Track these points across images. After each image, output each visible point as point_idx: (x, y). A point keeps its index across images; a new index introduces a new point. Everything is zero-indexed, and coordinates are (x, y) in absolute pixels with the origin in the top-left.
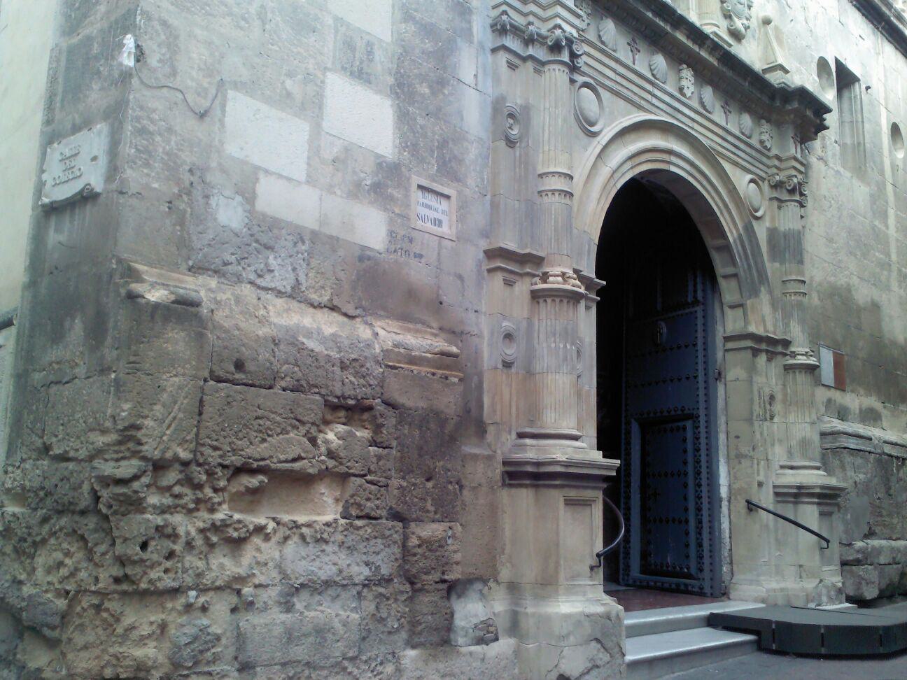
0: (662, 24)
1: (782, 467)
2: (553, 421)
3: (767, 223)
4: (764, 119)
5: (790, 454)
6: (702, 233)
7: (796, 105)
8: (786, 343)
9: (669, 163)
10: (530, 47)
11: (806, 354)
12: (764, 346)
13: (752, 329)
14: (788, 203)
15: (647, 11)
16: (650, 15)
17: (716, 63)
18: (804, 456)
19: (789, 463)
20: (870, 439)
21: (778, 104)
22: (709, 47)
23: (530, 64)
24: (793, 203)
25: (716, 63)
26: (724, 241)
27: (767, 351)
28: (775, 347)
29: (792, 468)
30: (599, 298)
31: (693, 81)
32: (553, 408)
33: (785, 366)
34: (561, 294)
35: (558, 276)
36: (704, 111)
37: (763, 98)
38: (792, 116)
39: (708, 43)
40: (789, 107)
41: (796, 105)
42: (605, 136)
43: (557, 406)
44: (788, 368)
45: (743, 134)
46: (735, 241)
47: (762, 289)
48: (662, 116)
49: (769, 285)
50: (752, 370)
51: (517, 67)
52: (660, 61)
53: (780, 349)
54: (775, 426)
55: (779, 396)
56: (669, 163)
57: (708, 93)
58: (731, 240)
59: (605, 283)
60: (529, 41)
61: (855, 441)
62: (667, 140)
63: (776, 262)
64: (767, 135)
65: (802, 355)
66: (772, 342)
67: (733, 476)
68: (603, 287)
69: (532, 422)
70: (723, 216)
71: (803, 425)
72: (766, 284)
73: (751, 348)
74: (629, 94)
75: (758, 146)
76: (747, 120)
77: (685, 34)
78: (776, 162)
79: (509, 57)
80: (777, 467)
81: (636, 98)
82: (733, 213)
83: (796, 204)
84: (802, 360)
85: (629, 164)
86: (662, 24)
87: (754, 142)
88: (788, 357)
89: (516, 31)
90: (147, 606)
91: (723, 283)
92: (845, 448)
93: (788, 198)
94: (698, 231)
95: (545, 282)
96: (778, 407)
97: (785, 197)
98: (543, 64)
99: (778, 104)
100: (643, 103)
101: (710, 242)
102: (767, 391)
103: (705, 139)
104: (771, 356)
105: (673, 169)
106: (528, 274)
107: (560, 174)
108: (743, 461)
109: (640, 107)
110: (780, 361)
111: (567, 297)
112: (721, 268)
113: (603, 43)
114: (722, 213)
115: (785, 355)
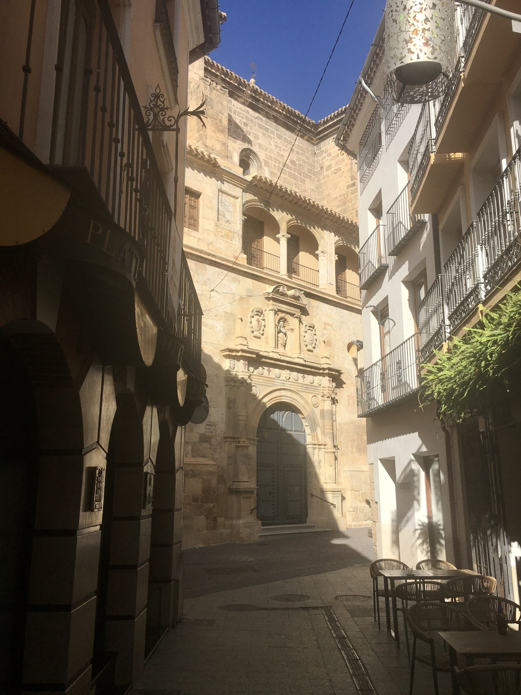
12: (317, 446)
105: (283, 400)
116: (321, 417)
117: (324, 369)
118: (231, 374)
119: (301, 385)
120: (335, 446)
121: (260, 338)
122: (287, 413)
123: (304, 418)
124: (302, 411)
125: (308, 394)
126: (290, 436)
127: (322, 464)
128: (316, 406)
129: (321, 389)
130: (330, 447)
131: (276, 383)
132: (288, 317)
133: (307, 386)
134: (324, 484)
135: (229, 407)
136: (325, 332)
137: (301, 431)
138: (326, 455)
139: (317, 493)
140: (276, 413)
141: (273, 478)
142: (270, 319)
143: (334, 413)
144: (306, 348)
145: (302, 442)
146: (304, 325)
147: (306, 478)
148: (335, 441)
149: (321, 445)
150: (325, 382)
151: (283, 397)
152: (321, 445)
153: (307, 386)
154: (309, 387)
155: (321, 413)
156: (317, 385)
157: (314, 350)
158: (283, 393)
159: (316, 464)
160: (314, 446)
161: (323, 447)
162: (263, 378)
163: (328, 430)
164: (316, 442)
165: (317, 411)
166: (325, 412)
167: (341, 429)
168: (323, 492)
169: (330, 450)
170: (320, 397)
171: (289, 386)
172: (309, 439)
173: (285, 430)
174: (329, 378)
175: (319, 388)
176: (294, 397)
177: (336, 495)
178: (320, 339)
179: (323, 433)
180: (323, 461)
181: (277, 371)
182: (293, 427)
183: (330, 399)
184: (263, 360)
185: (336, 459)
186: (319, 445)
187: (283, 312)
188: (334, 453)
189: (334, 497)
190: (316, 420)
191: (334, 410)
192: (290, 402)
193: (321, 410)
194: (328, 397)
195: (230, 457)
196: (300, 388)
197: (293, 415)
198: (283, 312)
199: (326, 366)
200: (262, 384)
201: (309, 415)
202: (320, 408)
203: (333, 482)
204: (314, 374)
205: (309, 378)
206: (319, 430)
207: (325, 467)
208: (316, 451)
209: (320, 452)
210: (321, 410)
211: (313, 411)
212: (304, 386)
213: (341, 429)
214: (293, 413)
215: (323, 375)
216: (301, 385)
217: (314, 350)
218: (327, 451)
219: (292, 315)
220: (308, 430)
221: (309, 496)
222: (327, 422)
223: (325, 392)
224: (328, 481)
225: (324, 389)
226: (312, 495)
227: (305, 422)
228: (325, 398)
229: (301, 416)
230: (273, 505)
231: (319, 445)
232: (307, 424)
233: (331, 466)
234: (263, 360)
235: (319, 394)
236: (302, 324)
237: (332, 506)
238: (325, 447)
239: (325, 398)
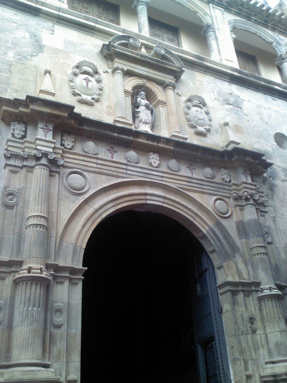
0: (125, 137)
1: (267, 363)
3: (235, 219)
4: (222, 167)
5: (270, 353)
6: (191, 231)
7: (236, 157)
8: (258, 284)
9: (146, 200)
10: (25, 162)
11: (270, 289)
12: (240, 288)
13: (230, 279)
14: (247, 206)
15: (113, 133)
16: (116, 135)
17: (172, 148)
18: (279, 354)
19: (270, 360)
20: (230, 337)
21: (226, 159)
22: (163, 141)
23: (24, 170)
24: (249, 206)
25: (172, 148)
26: (202, 233)
27: (243, 291)
28: (250, 288)
29: (273, 363)
30: (83, 278)
31: (158, 158)
33: (258, 297)
34: (24, 279)
36: (174, 172)
37: (216, 158)
38: (238, 163)
39: (162, 140)
40: (234, 159)
41: (236, 157)
42: (90, 193)
43: (24, 345)
44: (260, 299)
45: (206, 178)
46: (207, 231)
47: (236, 255)
48: (136, 178)
49: (240, 253)
50: (234, 303)
52: (132, 154)
53: (253, 288)
54: (258, 337)
55: (258, 318)
56: (146, 200)
57: (173, 163)
58: (205, 232)
59: (87, 268)
60: (24, 159)
62: (152, 191)
63: (243, 239)
64: (226, 175)
65: (267, 289)
66: (249, 285)
67: (235, 374)
68: (87, 271)
69: (8, 358)
71: (275, 333)
72: (238, 252)
73: (230, 291)
74: (105, 171)
75: (221, 181)
76: (208, 171)
77: (144, 139)
78: (235, 187)
80: (263, 363)
81: (115, 173)
82: (203, 217)
83: (251, 206)
84: (267, 292)
85: (111, 204)
86: (125, 137)
87: (217, 180)
88: (260, 292)
89: (15, 156)
91: (212, 256)
93: (245, 204)
94: (189, 231)
95: (29, 272)
96: (258, 324)
97: (244, 203)
98: (33, 167)
99: (226, 159)
100: (120, 174)
101: (197, 236)
102: (246, 316)
104: (248, 294)
105: (149, 202)
106: (12, 272)
107: (34, 216)
108: (237, 362)
110: (255, 295)
111: (30, 280)
112: (208, 249)
113: (86, 152)
114: (194, 219)
115: (258, 291)
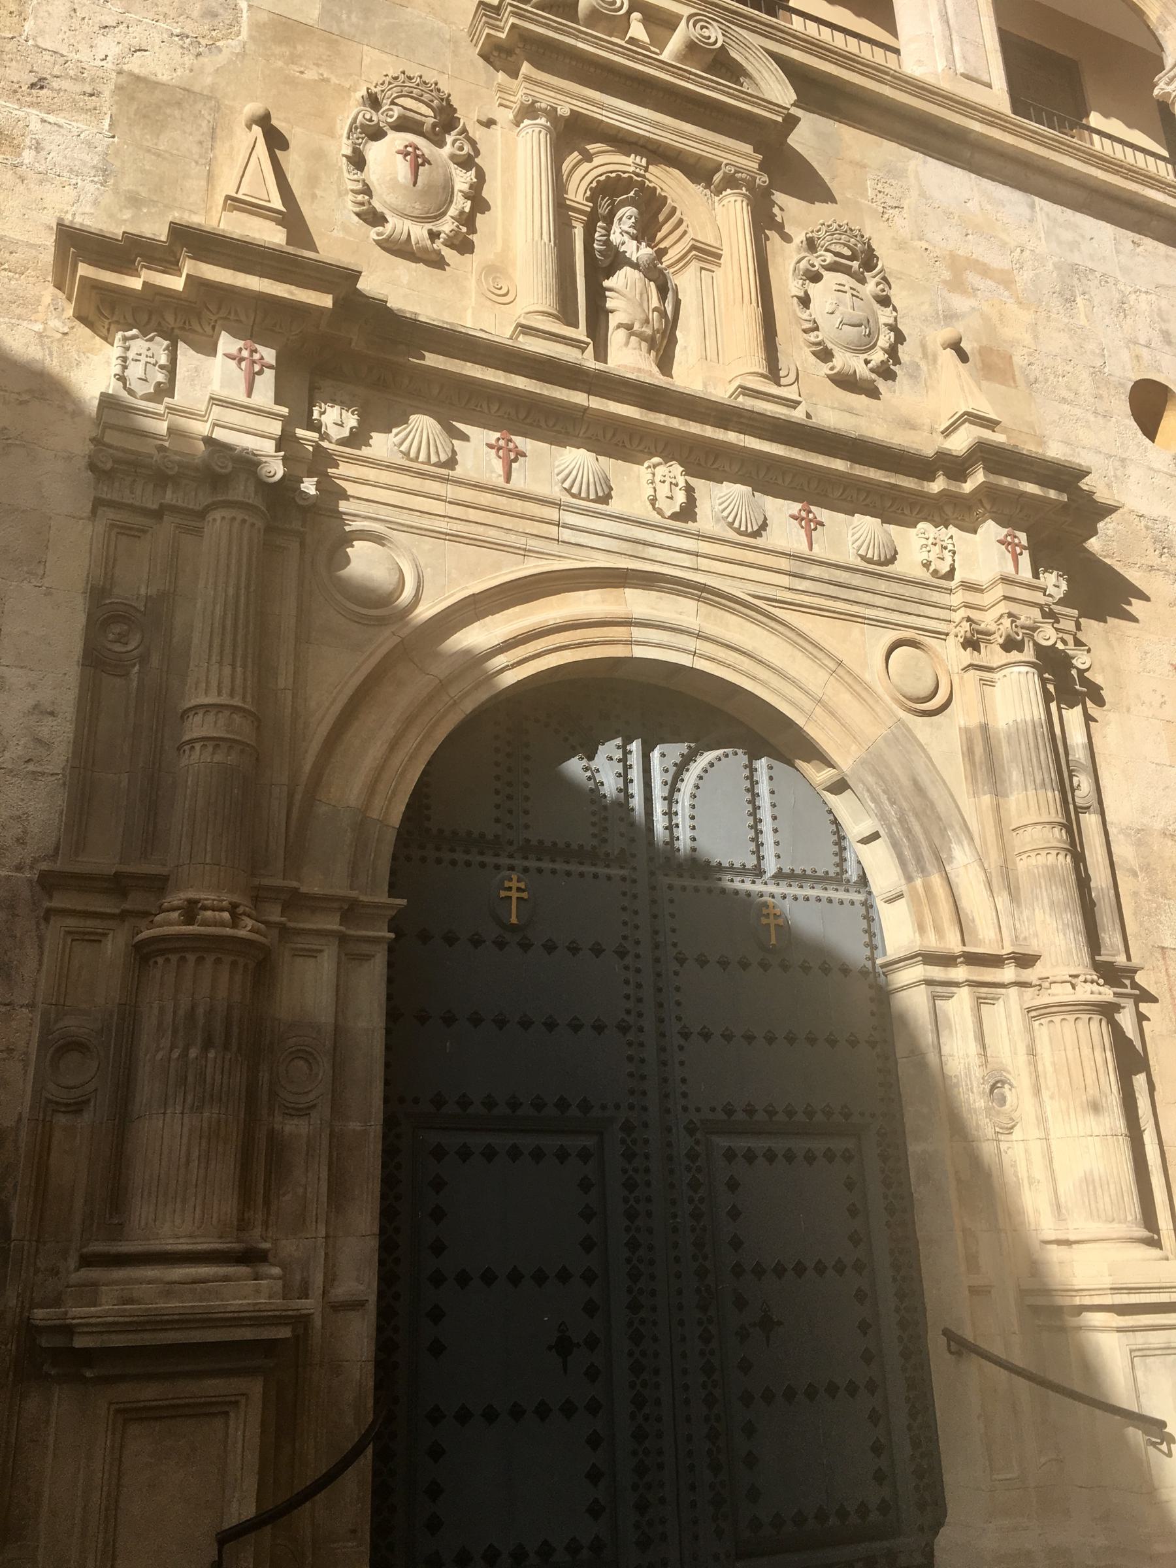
2: (143, 1223)
9: (630, 643)
12: (960, 973)
14: (1006, 671)
24: (1016, 669)
32: (1098, 1185)
35: (222, 910)
51: (144, 532)
56: (630, 643)
59: (404, 902)
61: (1043, 718)
68: (402, 911)
70: (764, 684)
79: (111, 516)
90: (767, 1323)
92: (835, 822)
100: (533, 544)
103: (729, 581)
105: (639, 652)
109: (526, 552)
116: (973, 779)
117: (957, 467)
118: (144, 434)
119: (784, 564)
120: (1110, 974)
121: (439, 263)
122: (710, 756)
123: (840, 786)
124: (812, 731)
125: (856, 629)
126: (749, 906)
127: (1019, 1097)
128: (929, 705)
129: (956, 599)
130: (1063, 972)
131: (566, 535)
132: (668, 182)
133: (843, 576)
134: (1056, 1254)
135: (96, 660)
136: (960, 303)
137: (837, 879)
138: (1042, 1030)
139: (998, 1328)
140: (610, 748)
141: (587, 1215)
142: (518, 163)
143: (1079, 754)
144: (825, 369)
145: (853, 949)
146: (799, 237)
147: (901, 1207)
148: (1110, 938)
149: (995, 961)
150: (985, 553)
151: (637, 633)
152: (995, 961)
153: (843, 576)
154: (857, 580)
155: (969, 753)
156: (924, 575)
157: (881, 384)
158: (636, 602)
159: (973, 1099)
160: (937, 973)
161: (1009, 973)
162: (450, 491)
163: (1039, 854)
164: (953, 944)
165: (942, 740)
166: (1006, 751)
167: (1147, 868)
168: (1049, 1313)
169: (1063, 994)
170: (953, 654)
171: (687, 560)
172: (899, 931)
173: (700, 869)
174: (1003, 532)
175: (936, 597)
176: (748, 645)
177: (1157, 1339)
178: (925, 335)
179: (1006, 881)
180: (1021, 1078)
181: (576, 460)
182: (769, 851)
183: (1029, 654)
184: (432, 360)
185: (1130, 1060)
186: (973, 959)
187: (623, 142)
188: (1107, 1011)
189: (1136, 1354)
190: (933, 793)
191: (1077, 737)
192: (685, 660)
193: (967, 732)
194: (1010, 645)
195: (73, 1046)
196: (785, 580)
197: (762, 776)
198: (623, 142)
199: (960, 443)
200: (441, 525)
201: (873, 762)
202: (962, 715)
203: (1120, 1229)
204: (898, 508)
205: (851, 534)
206: (963, 863)
207: (1042, 1121)
208: (959, 1005)
209: (995, 1015)
210: (967, 732)
211: (903, 738)
212: (815, 571)
213: (1147, 868)
214: (762, 764)
215: (957, 512)
216: (784, 564)
217: (881, 384)
218: (1044, 1000)
219: (699, 171)
220: (880, 865)
221: (936, 1344)
222: (1029, 805)
223: (987, 620)
224: (1079, 1225)
225: (972, 598)
226: (960, 1346)
227: (856, 819)
228: (993, 655)
229: (820, 776)
230: (594, 1442)
231: (973, 959)
232: (866, 826)
233: (1095, 1107)
234: (432, 360)
235: (942, 635)
236: (787, 238)
237: (1136, 1435)
238: (1030, 975)
239: (993, 655)
